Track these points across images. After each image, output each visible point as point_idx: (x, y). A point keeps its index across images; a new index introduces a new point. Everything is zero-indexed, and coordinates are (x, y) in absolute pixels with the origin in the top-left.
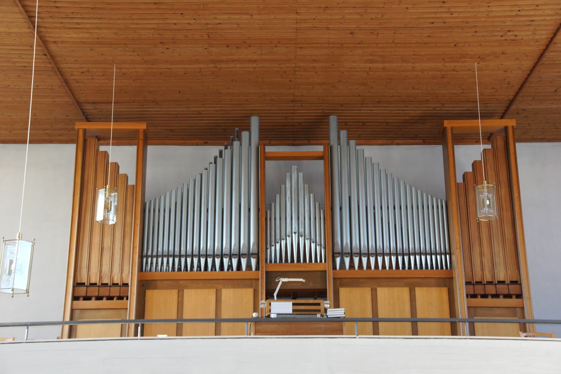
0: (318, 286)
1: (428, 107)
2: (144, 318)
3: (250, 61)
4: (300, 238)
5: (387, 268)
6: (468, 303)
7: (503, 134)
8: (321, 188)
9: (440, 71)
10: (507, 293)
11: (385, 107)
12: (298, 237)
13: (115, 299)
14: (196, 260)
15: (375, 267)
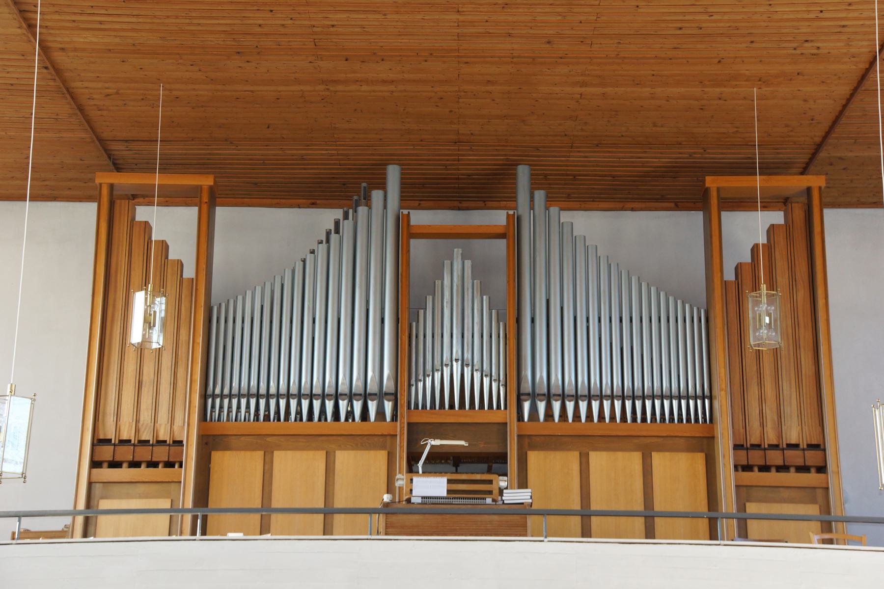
0: (493, 448)
1: (681, 153)
2: (207, 506)
3: (384, 82)
4: (465, 369)
5: (607, 420)
6: (736, 480)
7: (804, 199)
8: (500, 281)
9: (697, 100)
10: (803, 464)
11: (609, 152)
12: (462, 363)
13: (160, 466)
14: (293, 403)
15: (587, 417)
